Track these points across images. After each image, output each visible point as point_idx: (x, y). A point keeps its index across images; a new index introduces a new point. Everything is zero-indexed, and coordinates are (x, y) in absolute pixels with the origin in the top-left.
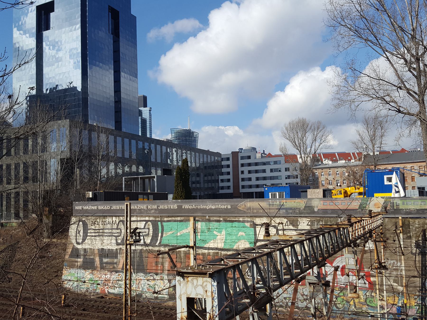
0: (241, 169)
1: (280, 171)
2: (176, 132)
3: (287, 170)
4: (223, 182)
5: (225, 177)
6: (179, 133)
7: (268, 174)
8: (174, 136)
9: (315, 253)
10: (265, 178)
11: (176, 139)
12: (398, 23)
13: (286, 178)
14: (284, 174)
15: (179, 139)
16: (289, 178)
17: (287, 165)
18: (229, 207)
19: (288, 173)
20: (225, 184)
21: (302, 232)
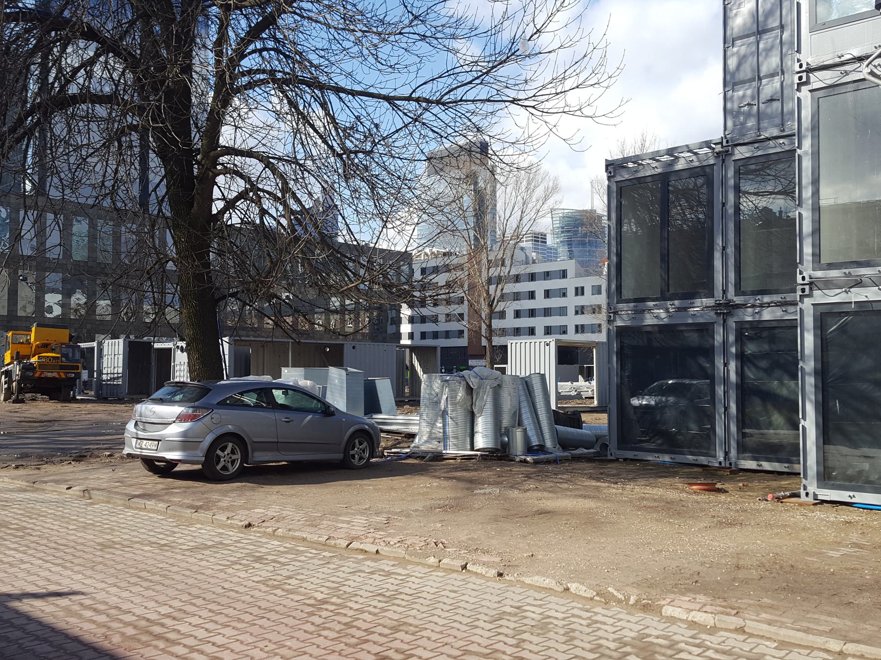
0: (602, 300)
1: (564, 295)
2: (564, 217)
3: (580, 290)
4: (583, 332)
5: (456, 309)
6: (571, 219)
7: (540, 303)
8: (558, 225)
9: (395, 558)
10: (532, 313)
11: (562, 232)
12: (761, 125)
13: (577, 313)
14: (572, 302)
15: (568, 232)
16: (583, 313)
17: (580, 282)
18: (653, 403)
19: (581, 301)
20: (454, 326)
21: (11, 487)
